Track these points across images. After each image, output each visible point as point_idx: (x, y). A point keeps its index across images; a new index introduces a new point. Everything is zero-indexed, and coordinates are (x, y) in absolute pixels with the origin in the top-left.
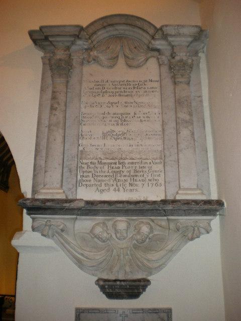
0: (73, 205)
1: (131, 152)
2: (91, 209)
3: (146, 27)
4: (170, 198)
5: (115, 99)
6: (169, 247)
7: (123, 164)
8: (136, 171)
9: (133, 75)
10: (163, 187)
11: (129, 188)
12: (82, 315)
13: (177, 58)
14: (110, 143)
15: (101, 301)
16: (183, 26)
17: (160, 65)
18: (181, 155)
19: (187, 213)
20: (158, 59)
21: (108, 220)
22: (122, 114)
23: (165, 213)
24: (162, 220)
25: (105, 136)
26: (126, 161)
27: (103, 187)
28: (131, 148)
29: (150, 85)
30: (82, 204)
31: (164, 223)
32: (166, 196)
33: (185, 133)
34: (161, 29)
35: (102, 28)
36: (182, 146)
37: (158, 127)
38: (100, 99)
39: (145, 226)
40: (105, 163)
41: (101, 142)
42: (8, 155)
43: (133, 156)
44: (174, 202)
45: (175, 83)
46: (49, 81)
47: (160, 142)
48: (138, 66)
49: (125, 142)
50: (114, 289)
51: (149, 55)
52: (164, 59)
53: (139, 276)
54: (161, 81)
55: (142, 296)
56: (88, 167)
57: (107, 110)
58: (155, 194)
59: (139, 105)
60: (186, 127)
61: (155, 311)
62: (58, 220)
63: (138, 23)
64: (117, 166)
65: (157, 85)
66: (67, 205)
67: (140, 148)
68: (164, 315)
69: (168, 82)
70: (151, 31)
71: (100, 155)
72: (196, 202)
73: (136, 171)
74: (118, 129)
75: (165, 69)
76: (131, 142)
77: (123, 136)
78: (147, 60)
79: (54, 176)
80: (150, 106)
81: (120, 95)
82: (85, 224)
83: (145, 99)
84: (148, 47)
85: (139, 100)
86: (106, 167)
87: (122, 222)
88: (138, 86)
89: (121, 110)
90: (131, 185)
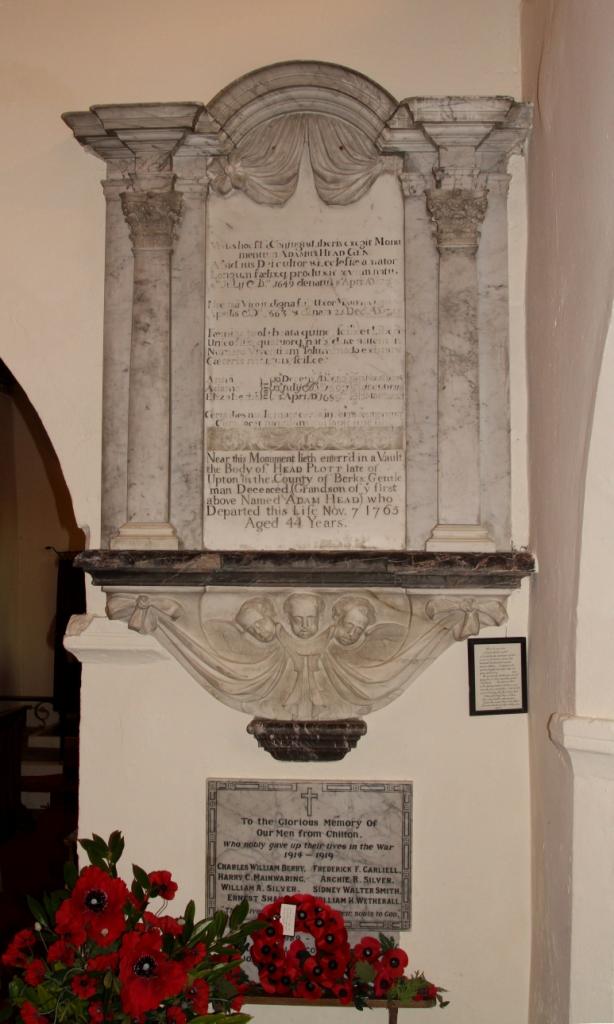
0: (193, 566)
1: (330, 431)
2: (238, 568)
4: (416, 546)
5: (288, 294)
7: (309, 460)
8: (339, 478)
9: (337, 226)
11: (321, 517)
12: (222, 796)
13: (448, 185)
14: (278, 408)
18: (445, 446)
22: (307, 334)
24: (396, 594)
25: (265, 391)
26: (317, 454)
27: (263, 517)
28: (327, 422)
29: (377, 252)
33: (457, 386)
34: (405, 105)
36: (448, 421)
38: (253, 294)
39: (356, 606)
41: (257, 407)
46: (126, 246)
47: (398, 405)
49: (318, 406)
51: (379, 167)
52: (416, 182)
56: (228, 468)
57: (270, 323)
58: (384, 536)
59: (350, 308)
60: (462, 373)
61: (377, 788)
62: (165, 597)
63: (349, 84)
64: (296, 464)
69: (423, 245)
71: (254, 438)
72: (471, 559)
73: (339, 478)
74: (298, 373)
75: (417, 208)
76: (329, 406)
77: (308, 390)
81: (303, 283)
82: (222, 602)
83: (362, 294)
87: (305, 600)
88: (348, 255)
89: (304, 323)
90: (327, 510)
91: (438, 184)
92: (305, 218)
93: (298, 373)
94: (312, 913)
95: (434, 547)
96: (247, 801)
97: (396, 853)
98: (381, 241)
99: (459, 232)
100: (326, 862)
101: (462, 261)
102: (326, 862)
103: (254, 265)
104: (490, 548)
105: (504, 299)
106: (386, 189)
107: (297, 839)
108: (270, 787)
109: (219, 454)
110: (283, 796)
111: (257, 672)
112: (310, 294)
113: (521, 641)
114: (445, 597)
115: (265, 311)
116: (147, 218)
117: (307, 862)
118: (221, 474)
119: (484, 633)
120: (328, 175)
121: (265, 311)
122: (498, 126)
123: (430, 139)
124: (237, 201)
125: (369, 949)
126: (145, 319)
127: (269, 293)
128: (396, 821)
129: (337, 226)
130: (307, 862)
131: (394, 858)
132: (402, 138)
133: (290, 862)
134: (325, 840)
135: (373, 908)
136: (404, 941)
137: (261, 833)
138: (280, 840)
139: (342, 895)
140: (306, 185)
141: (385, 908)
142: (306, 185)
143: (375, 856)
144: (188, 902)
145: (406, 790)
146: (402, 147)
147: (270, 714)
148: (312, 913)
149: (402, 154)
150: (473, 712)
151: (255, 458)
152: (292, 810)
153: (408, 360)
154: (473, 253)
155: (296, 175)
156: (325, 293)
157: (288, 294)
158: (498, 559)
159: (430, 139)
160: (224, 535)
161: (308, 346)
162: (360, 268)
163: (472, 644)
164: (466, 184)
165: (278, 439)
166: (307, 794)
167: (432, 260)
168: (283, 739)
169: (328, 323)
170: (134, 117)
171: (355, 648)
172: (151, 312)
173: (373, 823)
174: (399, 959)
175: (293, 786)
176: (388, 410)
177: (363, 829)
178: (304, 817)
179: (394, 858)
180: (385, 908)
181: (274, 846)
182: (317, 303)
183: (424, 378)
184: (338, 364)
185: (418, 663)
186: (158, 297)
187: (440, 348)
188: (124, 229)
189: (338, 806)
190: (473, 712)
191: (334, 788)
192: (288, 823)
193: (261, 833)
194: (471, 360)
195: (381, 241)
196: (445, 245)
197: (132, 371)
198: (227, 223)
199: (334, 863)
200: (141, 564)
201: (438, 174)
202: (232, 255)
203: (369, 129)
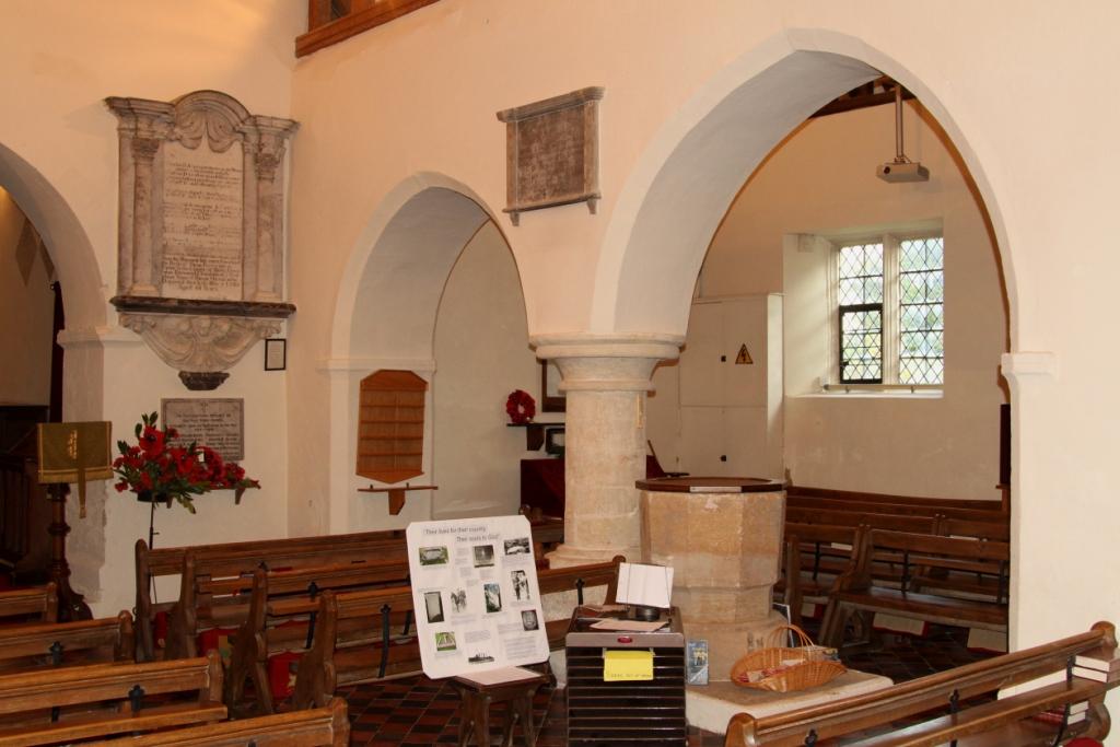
0: (167, 304)
1: (212, 249)
2: (182, 307)
3: (238, 109)
4: (247, 299)
5: (197, 189)
6: (245, 344)
7: (204, 261)
8: (216, 270)
9: (216, 161)
10: (240, 288)
11: (209, 286)
12: (169, 405)
13: (265, 151)
14: (192, 239)
15: (185, 393)
16: (276, 119)
17: (244, 154)
18: (261, 259)
19: (263, 315)
20: (243, 145)
21: (692, 656)
22: (204, 207)
23: (245, 314)
24: (240, 320)
25: (187, 230)
26: (208, 259)
27: (185, 285)
28: (211, 246)
29: (233, 175)
30: (175, 304)
31: (240, 322)
32: (243, 298)
33: (266, 235)
34: (255, 117)
35: (178, 103)
36: (263, 249)
37: (238, 223)
38: (182, 187)
39: (224, 325)
40: (186, 260)
41: (182, 237)
42: (411, 462)
43: (213, 254)
44: (256, 304)
45: (259, 178)
46: (131, 161)
47: (239, 241)
48: (221, 151)
49: (208, 238)
50: (195, 381)
51: (234, 138)
52: (251, 147)
53: (217, 369)
54: (244, 171)
55: (219, 388)
56: (171, 263)
57: (189, 201)
58: (234, 295)
59: (221, 198)
60: (268, 230)
61: (230, 401)
62: (149, 317)
63: (231, 103)
64: (199, 263)
65: (239, 175)
66: (162, 304)
67: (221, 246)
68: (237, 404)
69: (251, 175)
70: (243, 116)
71: (182, 250)
72: (274, 305)
73: (216, 270)
74: (201, 223)
75: (249, 158)
76: (213, 239)
77: (204, 231)
78: (231, 143)
79: (145, 272)
80: (232, 199)
81: (202, 184)
82: (174, 322)
83: (226, 192)
84: (234, 128)
85: (222, 192)
86: (188, 266)
87: (204, 321)
88: (221, 174)
89: (202, 202)
90: (211, 283)
91: (260, 150)
92: (203, 156)
93: (201, 223)
94: (209, 455)
95: (258, 300)
96: (180, 407)
97: (238, 427)
98: (234, 170)
99: (268, 171)
100: (211, 432)
101: (267, 183)
102: (211, 432)
103: (182, 174)
104: (278, 301)
105: (281, 200)
106: (236, 148)
107: (200, 423)
108: (189, 401)
109: (167, 256)
110: (193, 405)
111: (183, 350)
112: (205, 189)
113: (284, 340)
114: (258, 320)
115: (187, 195)
116: (141, 149)
117: (203, 433)
118: (168, 265)
119: (275, 336)
120: (215, 138)
121: (187, 195)
122: (286, 130)
123: (258, 130)
124: (176, 145)
125: (228, 468)
126: (142, 194)
127: (188, 187)
128: (238, 414)
129: (216, 161)
130: (203, 433)
131: (237, 430)
132: (248, 128)
133: (196, 433)
134: (210, 423)
135: (229, 451)
136: (241, 464)
137: (185, 421)
138: (192, 423)
139: (217, 446)
140: (205, 141)
141: (234, 451)
142: (205, 141)
143: (230, 429)
144: (579, 85)
145: (241, 402)
146: (245, 131)
147: (188, 369)
148: (209, 455)
149: (244, 134)
150: (266, 369)
151: (182, 259)
152: (197, 410)
153: (244, 222)
154: (272, 180)
155: (201, 138)
156: (210, 190)
157: (197, 189)
158: (283, 306)
159: (258, 130)
160: (171, 292)
161: (204, 212)
162: (224, 181)
163: (267, 341)
164: (272, 151)
165: (191, 251)
166: (203, 403)
167: (255, 182)
168: (195, 381)
169: (213, 203)
170: (144, 105)
171: (225, 341)
172: (144, 191)
173: (229, 416)
174: (241, 472)
175: (198, 401)
176: (234, 242)
177: (225, 419)
178: (202, 413)
179: (237, 430)
180: (234, 451)
181: (191, 426)
182: (208, 194)
183: (251, 230)
184: (216, 221)
185: (247, 348)
186: (147, 185)
187: (258, 219)
188: (129, 152)
189: (216, 408)
190: (266, 369)
191: (214, 401)
192: (196, 416)
193: (185, 421)
194: (271, 225)
195: (234, 170)
196: (397, 410)
197: (135, 218)
198: (172, 154)
199: (215, 432)
200: (148, 302)
201: (260, 146)
202: (173, 169)
203: (233, 122)
